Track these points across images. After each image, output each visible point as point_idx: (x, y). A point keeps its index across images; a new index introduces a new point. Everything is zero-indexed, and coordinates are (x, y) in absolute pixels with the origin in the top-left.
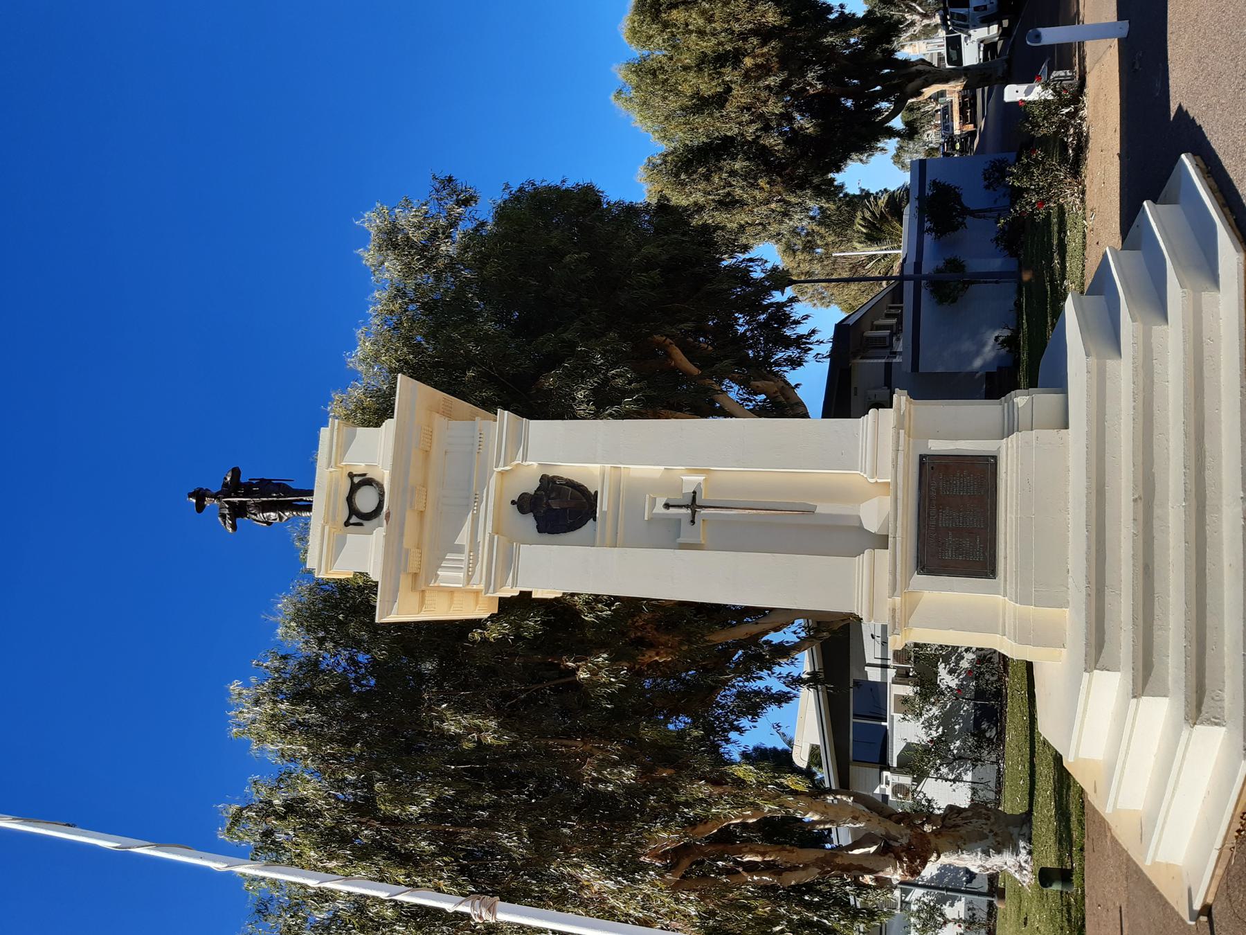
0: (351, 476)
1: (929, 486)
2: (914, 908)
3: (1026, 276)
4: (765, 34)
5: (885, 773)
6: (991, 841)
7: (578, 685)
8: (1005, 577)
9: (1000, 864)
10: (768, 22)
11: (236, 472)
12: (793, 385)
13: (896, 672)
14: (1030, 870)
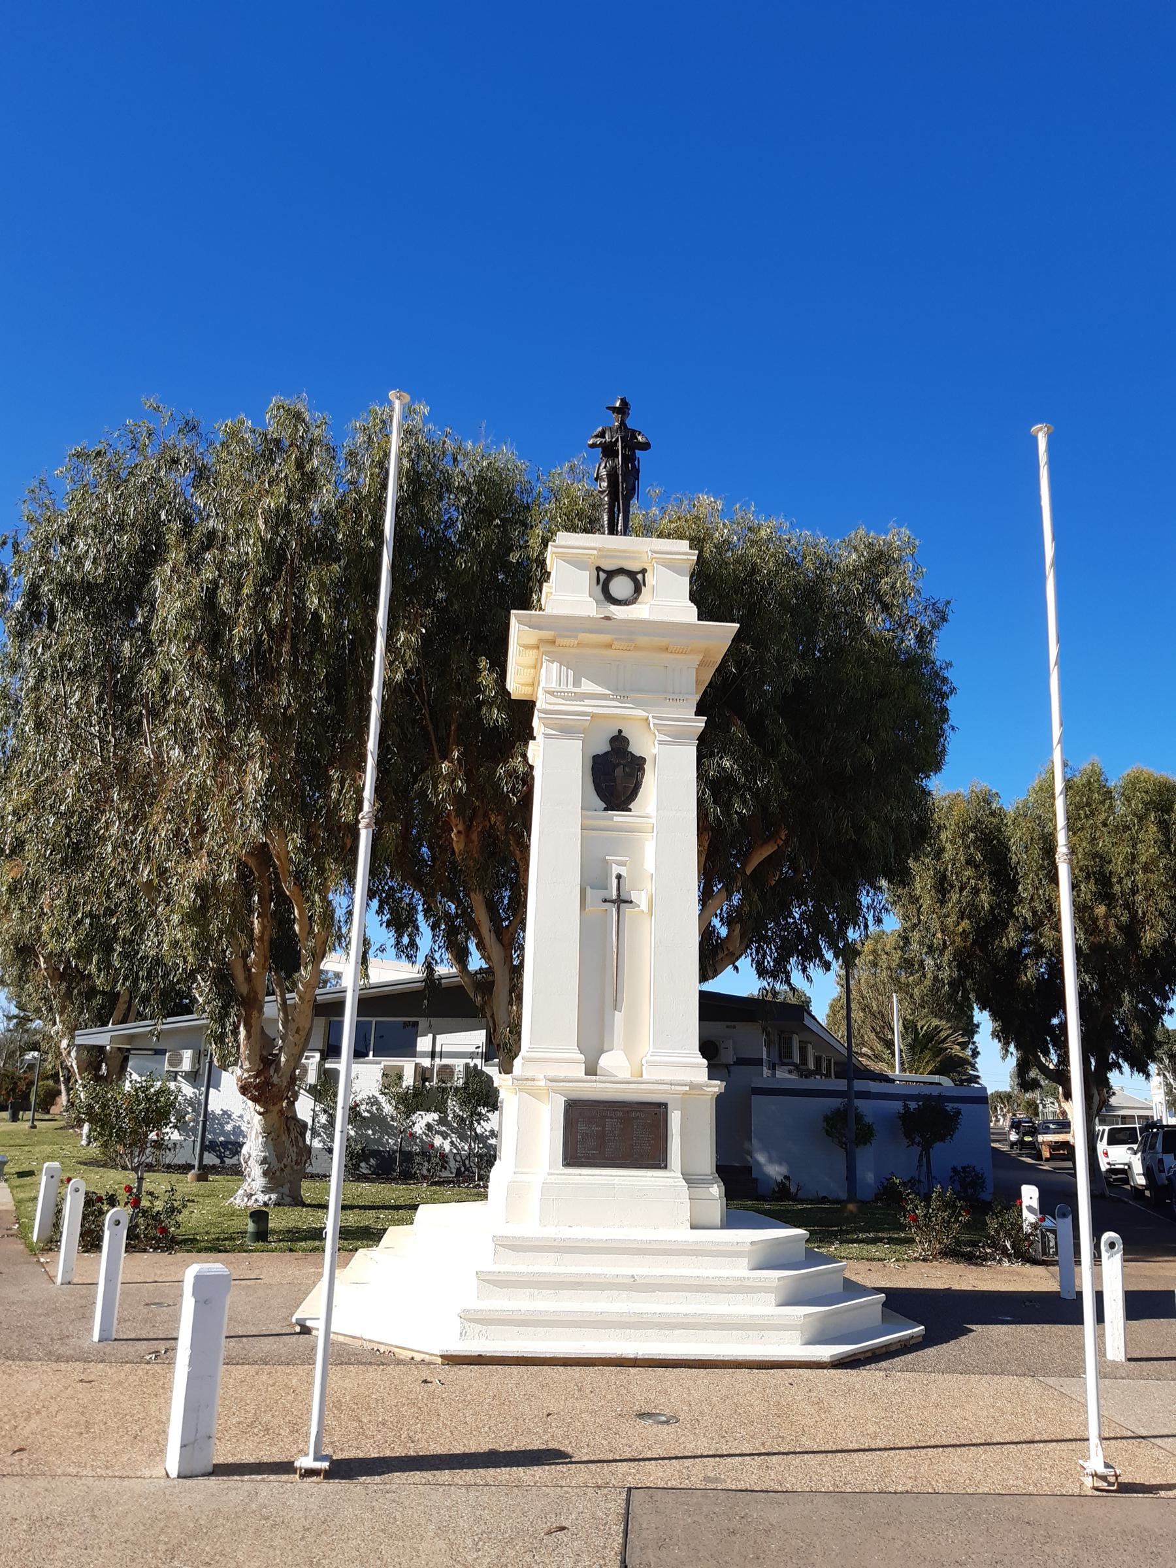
0: (644, 571)
1: (640, 1111)
2: (172, 1085)
3: (851, 1207)
4: (1132, 930)
5: (318, 1055)
6: (276, 1165)
7: (435, 764)
8: (564, 1174)
9: (253, 1174)
10: (1145, 932)
11: (646, 446)
12: (736, 964)
13: (427, 1068)
14: (249, 1204)
